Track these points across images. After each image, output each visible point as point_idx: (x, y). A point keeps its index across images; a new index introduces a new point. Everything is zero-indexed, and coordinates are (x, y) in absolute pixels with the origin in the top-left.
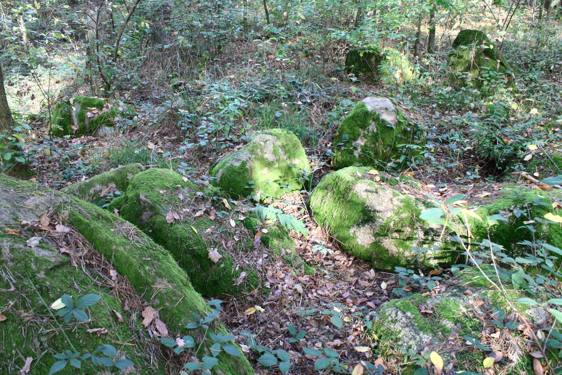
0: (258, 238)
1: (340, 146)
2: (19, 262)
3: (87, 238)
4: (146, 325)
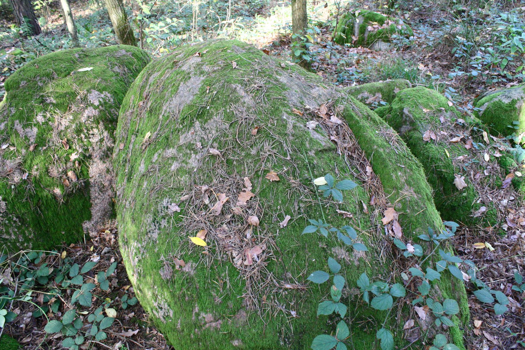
0: (509, 179)
3: (354, 132)
4: (385, 223)
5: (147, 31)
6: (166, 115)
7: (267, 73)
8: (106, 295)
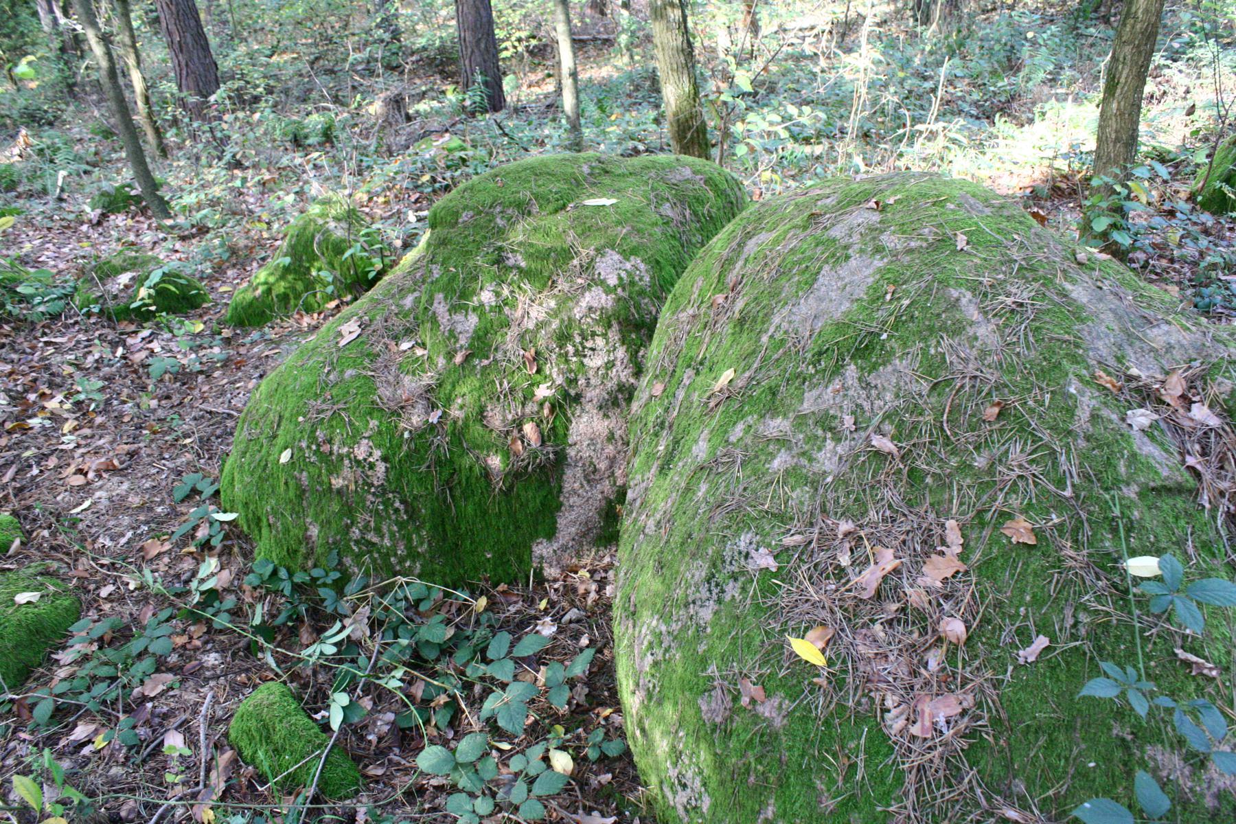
2: (1099, 447)
5: (738, 128)
6: (778, 336)
7: (1041, 273)
8: (557, 719)
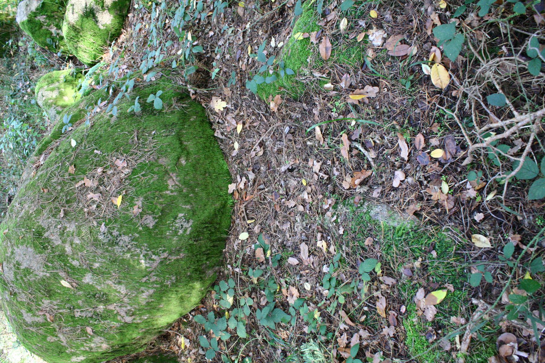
1: (56, 46)
